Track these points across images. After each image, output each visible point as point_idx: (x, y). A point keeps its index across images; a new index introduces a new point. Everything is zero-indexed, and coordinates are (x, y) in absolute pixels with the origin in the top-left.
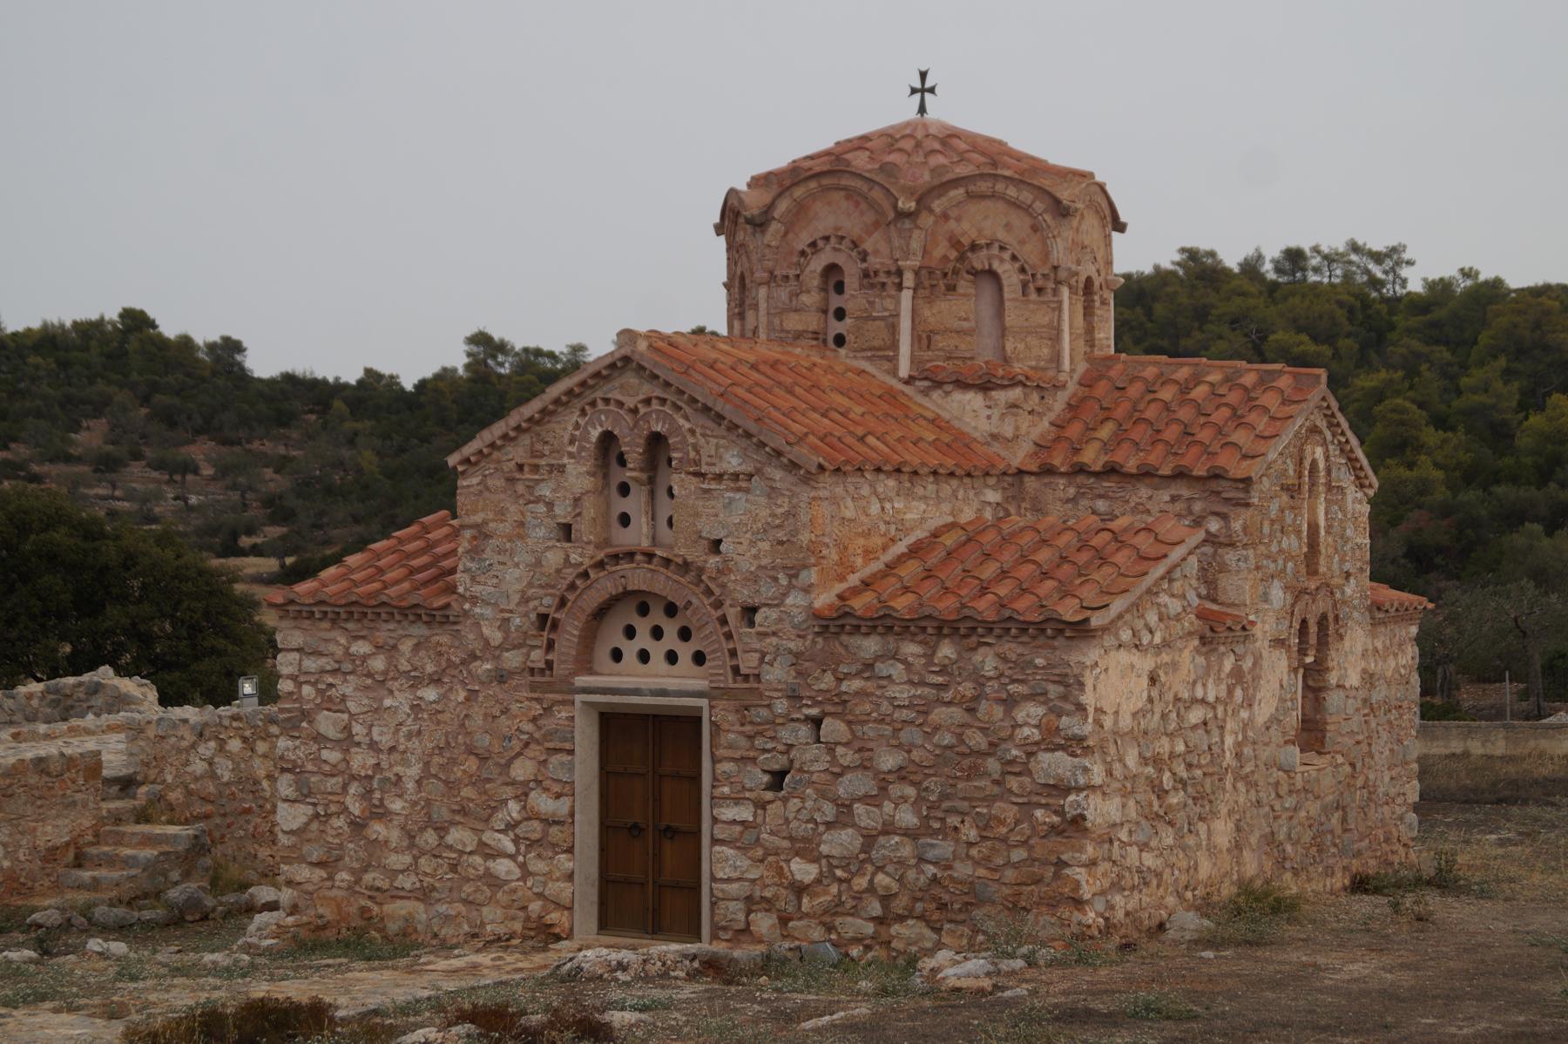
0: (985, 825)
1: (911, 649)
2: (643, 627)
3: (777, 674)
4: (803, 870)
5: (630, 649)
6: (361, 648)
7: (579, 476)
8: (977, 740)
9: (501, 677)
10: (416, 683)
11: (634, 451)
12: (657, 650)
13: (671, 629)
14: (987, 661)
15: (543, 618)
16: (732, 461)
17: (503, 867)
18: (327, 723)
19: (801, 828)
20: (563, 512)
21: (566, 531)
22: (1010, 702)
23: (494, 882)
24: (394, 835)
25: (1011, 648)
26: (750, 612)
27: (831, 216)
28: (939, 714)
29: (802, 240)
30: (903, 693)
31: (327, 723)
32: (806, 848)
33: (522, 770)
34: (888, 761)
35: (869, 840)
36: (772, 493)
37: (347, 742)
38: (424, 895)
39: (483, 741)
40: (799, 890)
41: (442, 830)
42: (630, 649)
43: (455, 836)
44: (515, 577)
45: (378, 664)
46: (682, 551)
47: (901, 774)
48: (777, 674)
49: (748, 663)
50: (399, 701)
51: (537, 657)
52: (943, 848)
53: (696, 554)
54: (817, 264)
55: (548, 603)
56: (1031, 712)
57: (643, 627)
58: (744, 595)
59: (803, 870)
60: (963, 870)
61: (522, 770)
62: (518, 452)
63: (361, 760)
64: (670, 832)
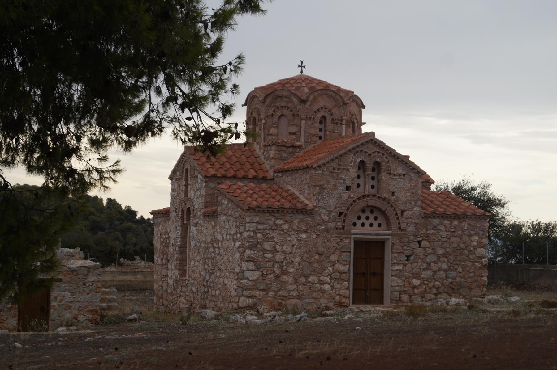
0: (464, 267)
1: (447, 222)
2: (363, 216)
3: (411, 229)
4: (416, 282)
5: (359, 223)
6: (280, 222)
7: (353, 172)
8: (462, 246)
9: (327, 230)
10: (299, 232)
11: (369, 165)
12: (367, 223)
13: (372, 217)
14: (465, 225)
15: (341, 213)
16: (400, 171)
17: (327, 287)
18: (267, 246)
19: (416, 270)
20: (348, 183)
21: (348, 188)
22: (470, 236)
23: (323, 291)
24: (291, 280)
25: (471, 222)
26: (403, 212)
27: (322, 102)
28: (453, 239)
29: (315, 108)
30: (444, 234)
31: (267, 246)
32: (417, 276)
33: (333, 258)
34: (440, 252)
35: (435, 273)
36: (411, 180)
37: (275, 250)
38: (299, 297)
39: (321, 250)
40: (414, 287)
41: (307, 277)
42: (359, 223)
43: (311, 279)
44: (332, 201)
45: (286, 227)
46: (384, 195)
47: (443, 255)
48: (411, 229)
49: (403, 226)
50: (293, 238)
51: (340, 224)
52: (453, 274)
53: (388, 196)
54: (319, 115)
55: (343, 209)
56: (476, 238)
57: (363, 216)
58: (402, 207)
59: (416, 282)
60: (458, 279)
61: (333, 258)
62: (334, 165)
63: (279, 257)
64: (374, 274)
